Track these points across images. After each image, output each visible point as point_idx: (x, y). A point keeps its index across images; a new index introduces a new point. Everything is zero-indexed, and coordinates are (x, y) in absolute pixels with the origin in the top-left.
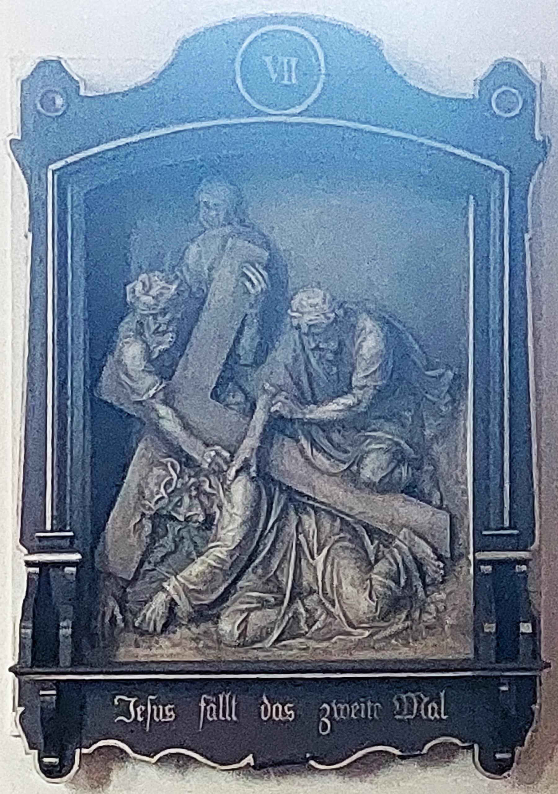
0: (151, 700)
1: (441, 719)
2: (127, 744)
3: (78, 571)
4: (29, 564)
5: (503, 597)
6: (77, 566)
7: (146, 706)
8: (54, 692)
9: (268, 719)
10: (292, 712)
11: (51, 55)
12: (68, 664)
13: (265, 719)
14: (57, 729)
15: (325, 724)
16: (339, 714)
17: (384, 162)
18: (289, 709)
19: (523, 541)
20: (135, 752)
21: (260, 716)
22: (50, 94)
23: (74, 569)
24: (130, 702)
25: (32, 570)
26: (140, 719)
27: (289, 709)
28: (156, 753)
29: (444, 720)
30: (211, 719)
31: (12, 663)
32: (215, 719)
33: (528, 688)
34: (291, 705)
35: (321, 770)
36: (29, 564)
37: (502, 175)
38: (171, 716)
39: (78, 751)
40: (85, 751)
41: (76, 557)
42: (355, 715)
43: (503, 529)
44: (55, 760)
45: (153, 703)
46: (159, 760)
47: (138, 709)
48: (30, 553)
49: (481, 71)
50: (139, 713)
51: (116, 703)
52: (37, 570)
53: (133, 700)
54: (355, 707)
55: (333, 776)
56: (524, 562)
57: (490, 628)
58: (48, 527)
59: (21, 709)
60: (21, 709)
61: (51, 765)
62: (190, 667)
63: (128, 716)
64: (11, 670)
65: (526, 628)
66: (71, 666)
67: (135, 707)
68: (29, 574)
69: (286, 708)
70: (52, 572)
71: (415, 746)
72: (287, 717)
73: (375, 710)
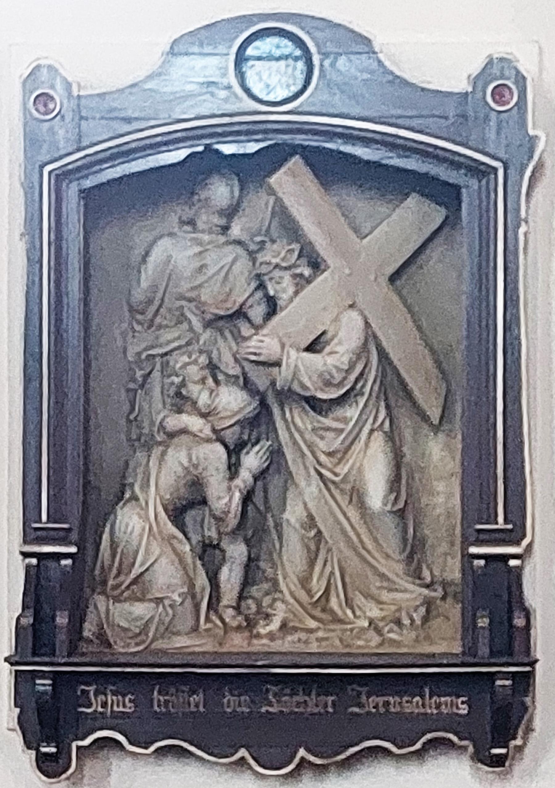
0: (111, 690)
1: (327, 712)
2: (126, 736)
4: (25, 555)
5: (495, 596)
6: (72, 558)
7: (106, 695)
8: (49, 682)
10: (465, 706)
11: (498, 52)
14: (51, 723)
16: (159, 706)
18: (130, 701)
19: (515, 534)
20: (131, 743)
21: (152, 706)
24: (88, 692)
25: (27, 560)
27: (463, 703)
28: (152, 743)
31: (7, 654)
33: (525, 682)
34: (464, 699)
36: (25, 555)
37: (495, 170)
38: (464, 710)
39: (74, 745)
41: (73, 549)
43: (497, 523)
44: (54, 750)
46: (156, 751)
49: (476, 68)
51: (79, 693)
52: (34, 561)
57: (483, 622)
61: (46, 754)
62: (368, 660)
64: (6, 660)
65: (519, 622)
67: (96, 695)
68: (28, 568)
70: (52, 564)
71: (416, 741)
72: (128, 710)
73: (351, 703)
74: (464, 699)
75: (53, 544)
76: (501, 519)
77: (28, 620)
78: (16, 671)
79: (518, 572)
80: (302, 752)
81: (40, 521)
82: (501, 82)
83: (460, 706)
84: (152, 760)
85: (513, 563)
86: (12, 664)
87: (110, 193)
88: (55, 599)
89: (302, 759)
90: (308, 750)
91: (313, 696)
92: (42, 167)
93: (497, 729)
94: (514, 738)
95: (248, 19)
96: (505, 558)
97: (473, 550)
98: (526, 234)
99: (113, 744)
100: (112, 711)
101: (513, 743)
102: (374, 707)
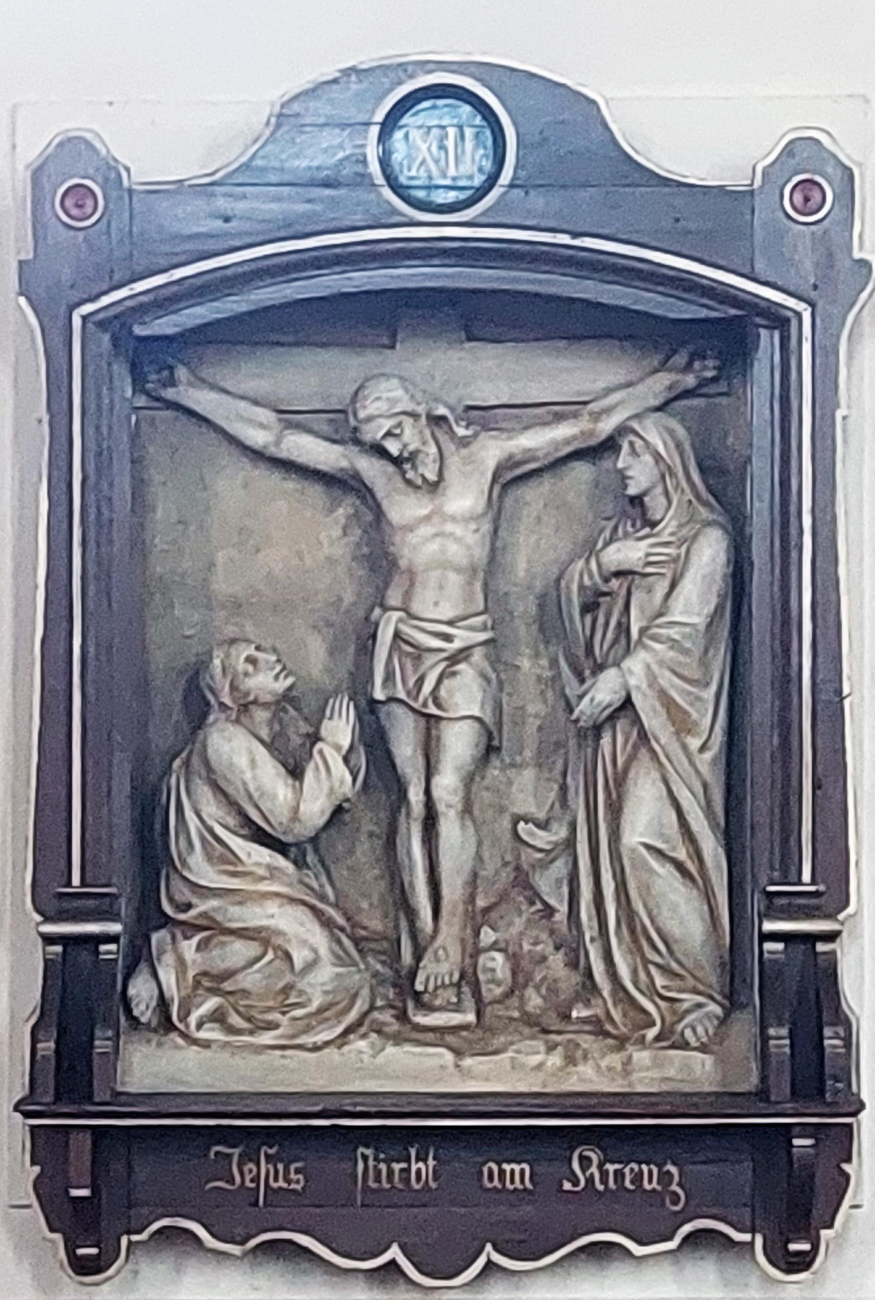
3: (65, 950)
4: (49, 939)
9: (423, 1188)
10: (301, 1177)
12: (49, 1099)
13: (417, 1187)
15: (675, 1194)
17: (400, 303)
20: (641, 1243)
22: (77, 187)
23: (113, 947)
24: (229, 1156)
26: (249, 1184)
27: (297, 1171)
29: (508, 1190)
30: (511, 1187)
32: (387, 1186)
33: (840, 1142)
34: (299, 1165)
35: (514, 1273)
40: (135, 1238)
42: (632, 1182)
43: (800, 883)
45: (268, 1157)
47: (246, 1169)
48: (47, 919)
50: (248, 1178)
52: (58, 949)
53: (236, 1151)
54: (251, 1171)
55: (543, 1279)
56: (832, 937)
58: (76, 880)
59: (37, 1169)
60: (37, 1169)
63: (232, 1181)
64: (16, 1108)
66: (54, 1103)
69: (292, 1168)
70: (84, 956)
72: (293, 1186)
74: (299, 1165)
75: (791, 918)
76: (806, 876)
77: (48, 1047)
78: (33, 1128)
79: (832, 960)
80: (394, 1252)
81: (69, 884)
82: (809, 174)
83: (293, 1176)
84: (246, 1266)
85: (821, 947)
86: (27, 1115)
87: (160, 324)
88: (79, 1010)
89: (393, 1263)
90: (496, 1248)
91: (431, 1162)
92: (812, 305)
93: (792, 1212)
94: (830, 1226)
95: (405, 69)
96: (812, 938)
97: (769, 926)
98: (844, 418)
99: (722, 1240)
100: (366, 1188)
101: (825, 1233)
102: (252, 1181)
